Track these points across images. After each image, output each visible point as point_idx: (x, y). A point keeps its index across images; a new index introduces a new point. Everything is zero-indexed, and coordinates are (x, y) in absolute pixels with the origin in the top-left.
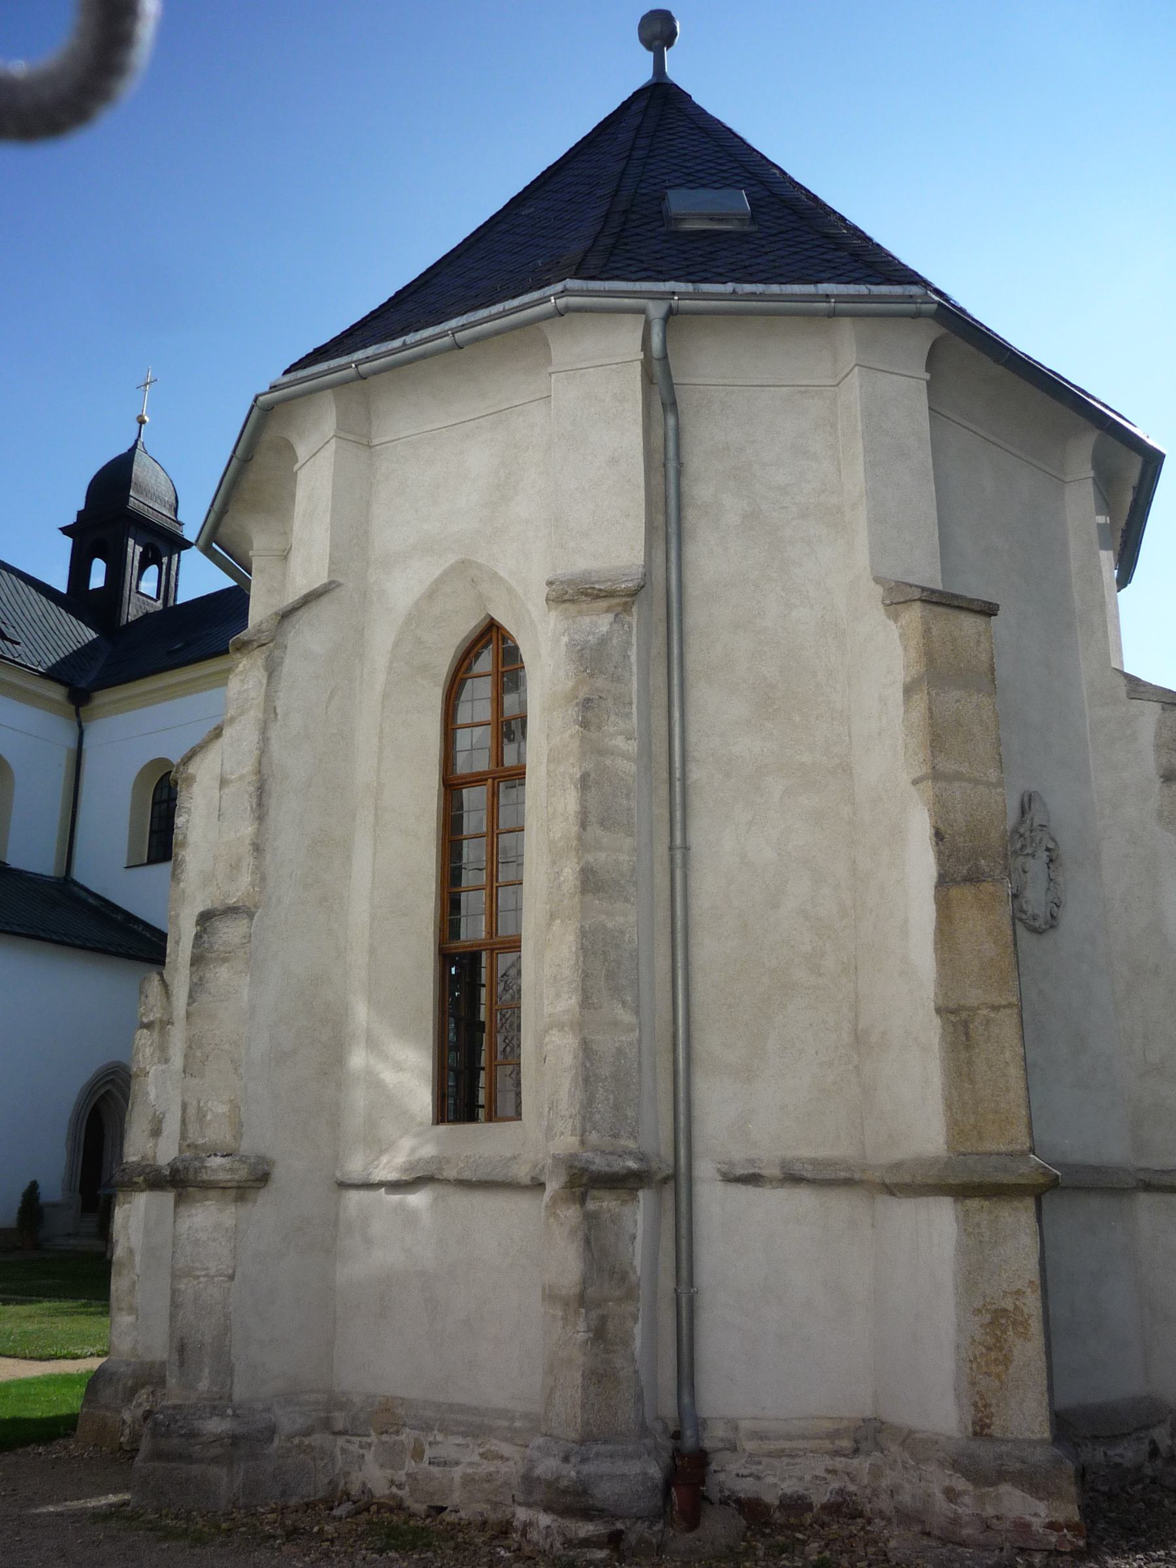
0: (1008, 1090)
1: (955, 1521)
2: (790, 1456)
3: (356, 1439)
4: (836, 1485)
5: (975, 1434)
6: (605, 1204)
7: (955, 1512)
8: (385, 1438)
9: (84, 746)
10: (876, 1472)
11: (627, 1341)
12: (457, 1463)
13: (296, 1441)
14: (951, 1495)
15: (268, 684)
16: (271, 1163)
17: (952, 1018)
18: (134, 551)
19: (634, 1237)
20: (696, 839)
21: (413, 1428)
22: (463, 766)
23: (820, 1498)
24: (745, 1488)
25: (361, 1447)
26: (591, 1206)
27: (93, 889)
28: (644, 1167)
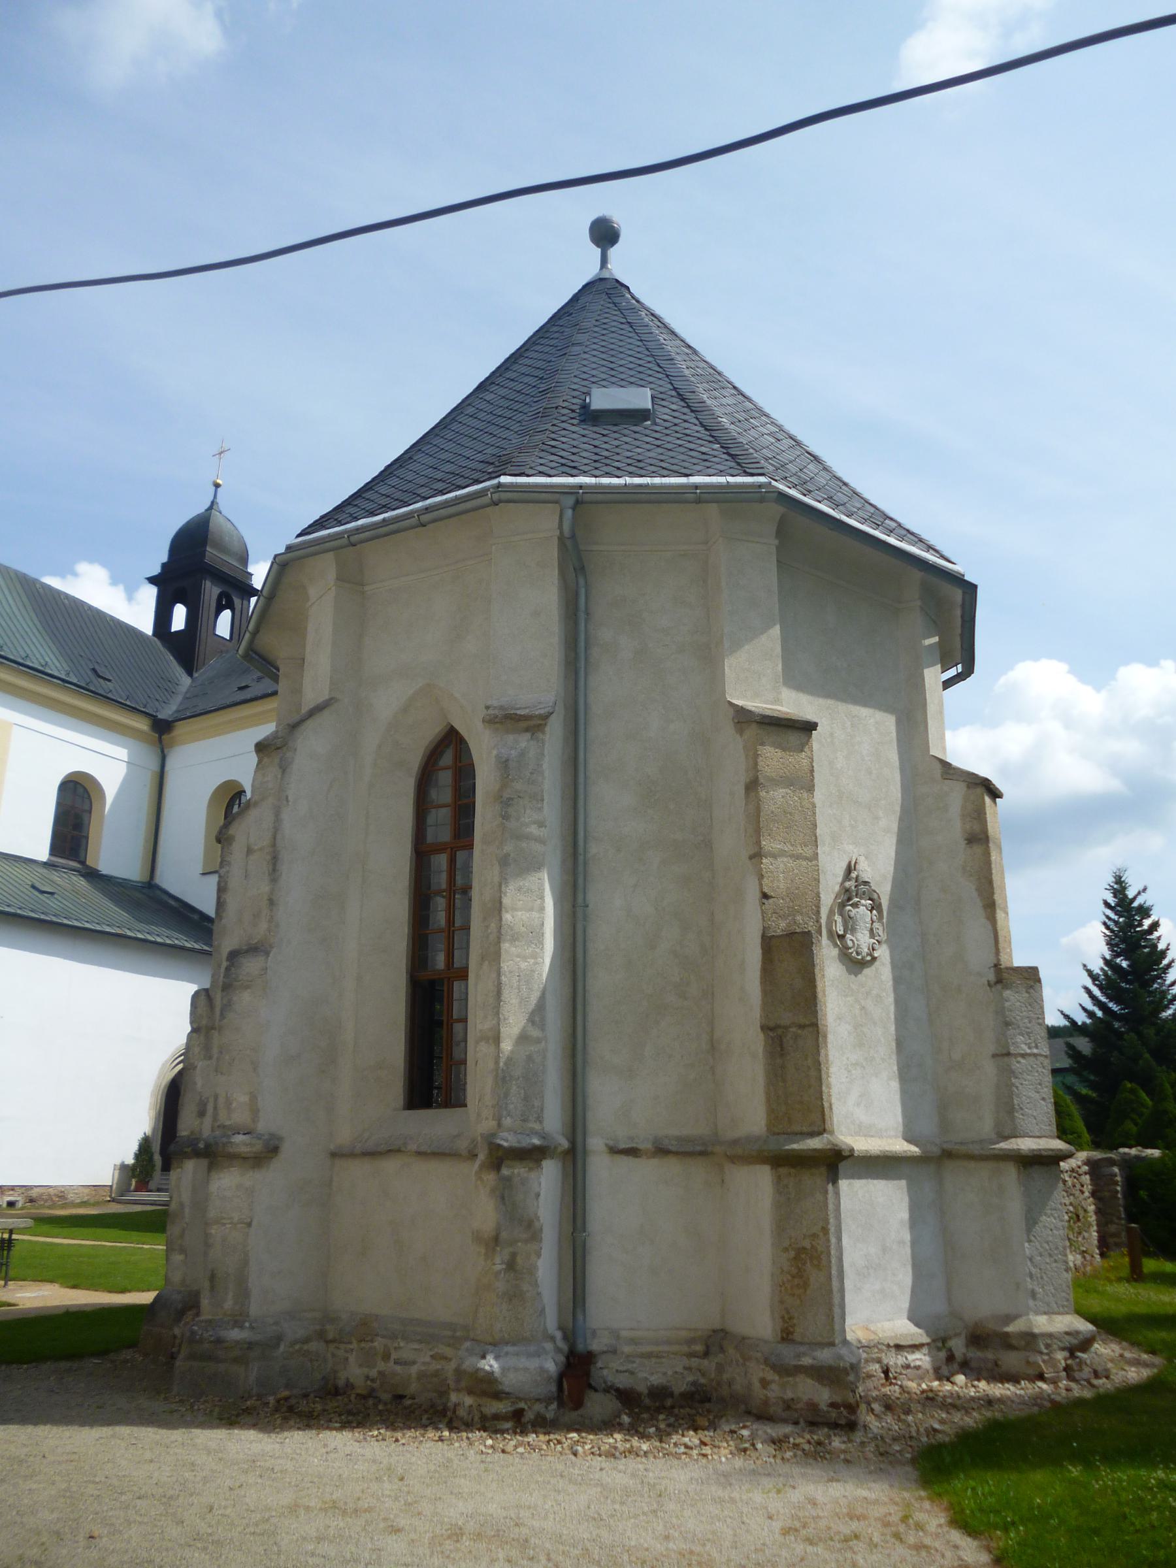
0: (810, 1087)
1: (766, 1402)
2: (657, 1357)
3: (342, 1346)
4: (690, 1378)
5: (783, 1339)
6: (516, 1171)
7: (766, 1396)
8: (363, 1345)
9: (167, 768)
10: (720, 1368)
11: (532, 1271)
12: (414, 1363)
13: (297, 1347)
14: (764, 1383)
15: (282, 779)
16: (281, 1139)
17: (771, 1034)
18: (211, 591)
19: (538, 1195)
20: (592, 898)
21: (383, 1337)
22: (430, 838)
23: (680, 1387)
24: (622, 1382)
25: (346, 1351)
26: (505, 1171)
27: (172, 891)
28: (545, 1144)
